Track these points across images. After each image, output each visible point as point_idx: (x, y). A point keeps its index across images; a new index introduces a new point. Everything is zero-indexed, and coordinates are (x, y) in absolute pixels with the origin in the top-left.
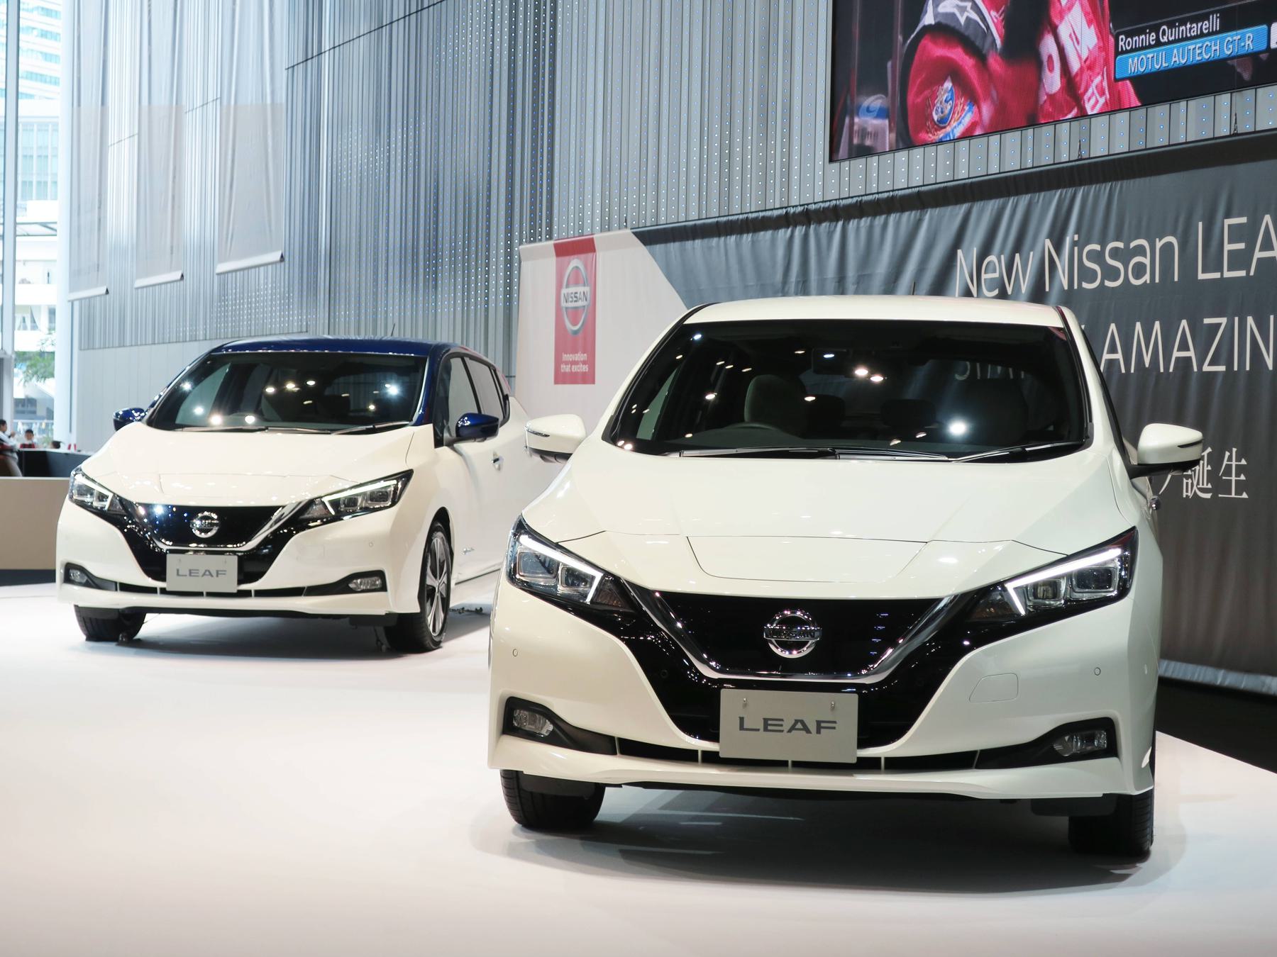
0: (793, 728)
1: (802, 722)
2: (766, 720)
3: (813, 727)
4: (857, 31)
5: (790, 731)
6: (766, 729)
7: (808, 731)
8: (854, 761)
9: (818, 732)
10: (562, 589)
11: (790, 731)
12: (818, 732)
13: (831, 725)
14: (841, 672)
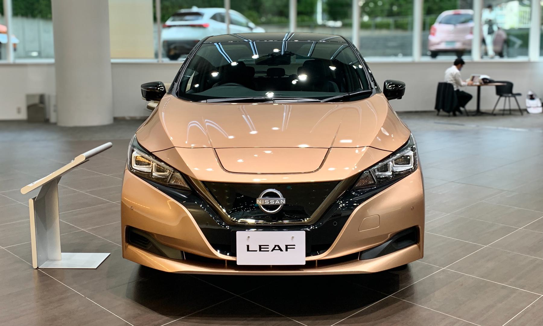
0: (274, 249)
1: (278, 246)
2: (260, 246)
3: (284, 248)
4: (163, 119)
5: (272, 251)
6: (260, 250)
7: (281, 250)
8: (304, 263)
9: (287, 250)
10: (155, 174)
11: (272, 251)
12: (287, 250)
13: (293, 247)
14: (299, 219)
